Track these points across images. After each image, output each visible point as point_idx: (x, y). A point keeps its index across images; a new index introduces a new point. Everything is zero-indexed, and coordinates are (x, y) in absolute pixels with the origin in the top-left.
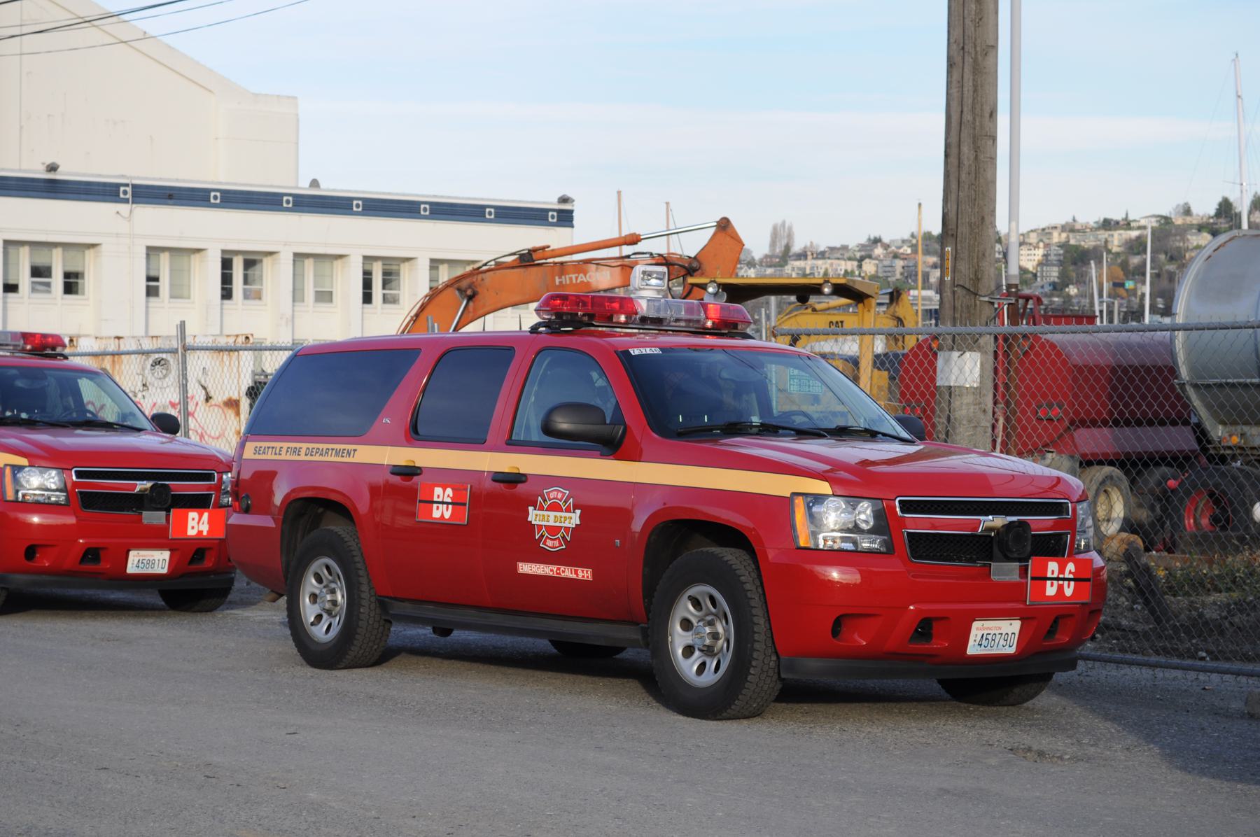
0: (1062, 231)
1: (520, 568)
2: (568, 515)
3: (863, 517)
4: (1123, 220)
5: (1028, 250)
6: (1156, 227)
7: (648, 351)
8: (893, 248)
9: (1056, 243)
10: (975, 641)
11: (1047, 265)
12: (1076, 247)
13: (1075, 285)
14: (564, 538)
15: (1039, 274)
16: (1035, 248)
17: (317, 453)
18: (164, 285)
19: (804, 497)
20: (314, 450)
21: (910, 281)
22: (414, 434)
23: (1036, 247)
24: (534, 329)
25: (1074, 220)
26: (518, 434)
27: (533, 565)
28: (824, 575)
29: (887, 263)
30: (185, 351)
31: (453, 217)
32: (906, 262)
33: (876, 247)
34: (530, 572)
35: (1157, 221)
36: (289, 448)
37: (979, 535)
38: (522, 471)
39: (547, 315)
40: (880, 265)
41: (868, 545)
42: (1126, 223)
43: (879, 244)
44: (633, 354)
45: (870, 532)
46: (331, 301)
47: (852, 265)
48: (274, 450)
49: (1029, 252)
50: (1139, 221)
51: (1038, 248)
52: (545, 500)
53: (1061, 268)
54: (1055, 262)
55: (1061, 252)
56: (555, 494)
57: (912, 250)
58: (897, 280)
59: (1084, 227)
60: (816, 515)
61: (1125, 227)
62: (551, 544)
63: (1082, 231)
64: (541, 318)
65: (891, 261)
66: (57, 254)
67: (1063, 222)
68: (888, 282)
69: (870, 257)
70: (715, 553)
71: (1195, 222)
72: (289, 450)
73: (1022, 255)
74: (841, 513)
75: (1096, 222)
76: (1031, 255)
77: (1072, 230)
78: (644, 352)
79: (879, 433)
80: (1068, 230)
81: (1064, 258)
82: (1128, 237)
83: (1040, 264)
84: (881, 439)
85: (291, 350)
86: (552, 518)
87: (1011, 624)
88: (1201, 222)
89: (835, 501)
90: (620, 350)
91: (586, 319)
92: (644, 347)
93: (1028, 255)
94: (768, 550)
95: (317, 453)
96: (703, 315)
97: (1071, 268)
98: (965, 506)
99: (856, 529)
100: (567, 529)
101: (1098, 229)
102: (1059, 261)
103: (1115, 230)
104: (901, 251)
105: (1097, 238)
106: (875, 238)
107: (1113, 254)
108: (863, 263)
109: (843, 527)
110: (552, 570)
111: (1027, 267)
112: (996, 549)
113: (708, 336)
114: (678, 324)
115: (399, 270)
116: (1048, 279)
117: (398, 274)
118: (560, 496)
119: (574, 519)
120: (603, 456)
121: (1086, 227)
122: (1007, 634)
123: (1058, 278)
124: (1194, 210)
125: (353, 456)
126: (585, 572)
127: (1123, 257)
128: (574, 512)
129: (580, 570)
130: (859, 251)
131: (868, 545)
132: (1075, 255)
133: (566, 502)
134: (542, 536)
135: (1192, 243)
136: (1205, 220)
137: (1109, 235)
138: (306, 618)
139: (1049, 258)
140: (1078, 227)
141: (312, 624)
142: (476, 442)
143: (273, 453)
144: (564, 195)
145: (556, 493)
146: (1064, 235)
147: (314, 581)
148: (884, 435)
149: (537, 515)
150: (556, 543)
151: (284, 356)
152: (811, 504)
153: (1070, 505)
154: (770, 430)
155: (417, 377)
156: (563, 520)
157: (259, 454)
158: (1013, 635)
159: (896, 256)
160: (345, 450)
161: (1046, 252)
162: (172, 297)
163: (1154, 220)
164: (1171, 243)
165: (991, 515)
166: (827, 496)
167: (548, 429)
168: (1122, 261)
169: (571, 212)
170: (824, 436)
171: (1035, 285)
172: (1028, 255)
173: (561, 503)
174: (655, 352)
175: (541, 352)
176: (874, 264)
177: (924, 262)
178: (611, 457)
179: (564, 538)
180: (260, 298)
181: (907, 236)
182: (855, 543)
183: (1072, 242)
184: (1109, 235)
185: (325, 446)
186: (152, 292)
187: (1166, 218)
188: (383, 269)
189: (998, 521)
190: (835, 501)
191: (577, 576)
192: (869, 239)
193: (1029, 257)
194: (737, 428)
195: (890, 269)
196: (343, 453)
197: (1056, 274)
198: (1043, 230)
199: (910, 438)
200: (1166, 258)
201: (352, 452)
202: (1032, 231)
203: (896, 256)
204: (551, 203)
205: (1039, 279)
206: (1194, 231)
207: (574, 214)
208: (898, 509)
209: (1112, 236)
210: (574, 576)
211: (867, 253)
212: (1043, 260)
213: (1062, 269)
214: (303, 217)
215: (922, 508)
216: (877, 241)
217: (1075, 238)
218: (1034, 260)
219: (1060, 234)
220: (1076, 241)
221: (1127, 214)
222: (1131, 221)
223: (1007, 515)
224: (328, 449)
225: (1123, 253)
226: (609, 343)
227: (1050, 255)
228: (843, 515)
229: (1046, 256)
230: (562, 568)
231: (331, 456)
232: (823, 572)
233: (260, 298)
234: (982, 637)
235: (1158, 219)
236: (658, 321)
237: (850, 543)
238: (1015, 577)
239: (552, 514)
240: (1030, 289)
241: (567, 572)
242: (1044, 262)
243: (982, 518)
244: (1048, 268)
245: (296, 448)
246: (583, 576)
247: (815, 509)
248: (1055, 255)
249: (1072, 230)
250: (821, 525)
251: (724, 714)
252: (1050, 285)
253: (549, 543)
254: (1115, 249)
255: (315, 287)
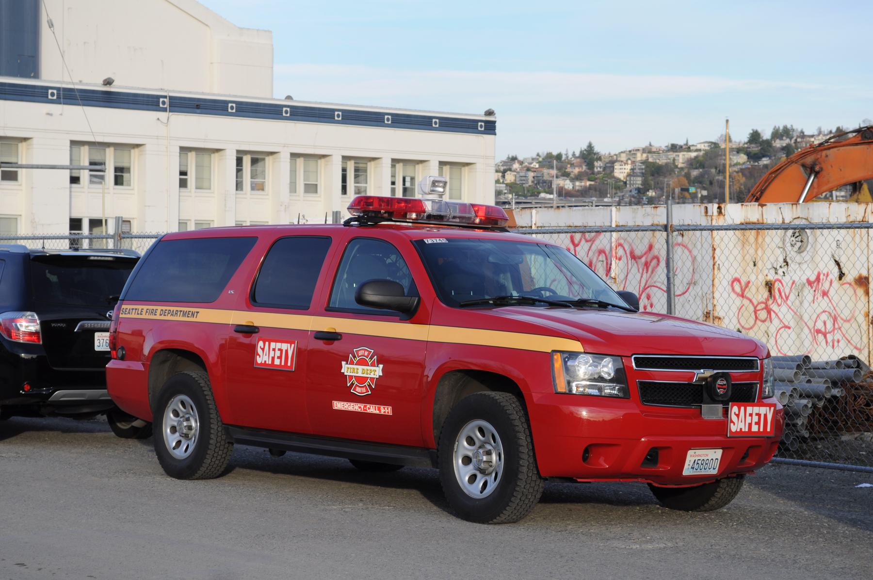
0: (643, 153)
1: (335, 405)
2: (373, 368)
3: (606, 369)
4: (685, 145)
5: (620, 165)
6: (708, 150)
7: (438, 241)
8: (526, 164)
9: (639, 161)
10: (689, 465)
11: (634, 176)
12: (654, 164)
13: (653, 190)
14: (370, 386)
15: (628, 182)
16: (625, 164)
17: (168, 313)
18: (191, 178)
19: (561, 354)
20: (167, 312)
21: (538, 187)
22: (253, 302)
23: (626, 164)
24: (347, 223)
25: (650, 145)
26: (335, 303)
27: (345, 403)
28: (577, 413)
29: (522, 174)
30: (121, 239)
31: (409, 126)
32: (535, 173)
33: (514, 163)
34: (343, 409)
35: (709, 146)
36: (148, 309)
37: (694, 385)
38: (255, 325)
39: (356, 213)
40: (518, 176)
41: (610, 391)
42: (687, 147)
43: (516, 161)
44: (427, 243)
45: (611, 381)
46: (316, 192)
47: (498, 176)
48: (137, 311)
49: (621, 167)
50: (696, 146)
51: (628, 164)
52: (354, 357)
53: (643, 178)
54: (639, 174)
55: (643, 167)
56: (363, 352)
57: (539, 165)
58: (530, 186)
59: (658, 150)
60: (570, 368)
61: (686, 150)
62: (359, 391)
63: (657, 152)
64: (351, 214)
65: (525, 172)
66: (110, 152)
67: (644, 146)
68: (524, 188)
69: (510, 170)
70: (491, 396)
71: (734, 146)
72: (148, 311)
73: (616, 169)
74: (589, 366)
75: (666, 147)
76: (622, 169)
77: (650, 152)
78: (435, 242)
79: (609, 304)
80: (647, 151)
81: (646, 171)
82: (689, 157)
83: (629, 175)
84: (611, 309)
85: (155, 238)
86: (360, 371)
87: (715, 452)
88: (738, 146)
89: (584, 357)
90: (414, 240)
91: (386, 215)
92: (435, 237)
93: (620, 169)
94: (533, 394)
95: (168, 313)
96: (473, 214)
97: (650, 178)
98: (678, 362)
99: (601, 379)
100: (372, 379)
101: (668, 151)
102: (642, 173)
103: (680, 152)
104: (532, 166)
105: (667, 157)
106: (513, 157)
107: (679, 168)
108: (506, 174)
109: (591, 377)
110: (360, 407)
111: (620, 177)
112: (705, 395)
113: (476, 230)
114: (454, 220)
115: (367, 167)
116: (634, 185)
117: (365, 171)
118: (366, 354)
119: (377, 371)
120: (402, 320)
121: (659, 150)
122: (717, 459)
123: (642, 185)
124: (734, 139)
125: (196, 317)
126: (386, 409)
127: (686, 171)
128: (377, 366)
129: (382, 407)
130: (502, 166)
131: (610, 391)
132: (653, 169)
133: (371, 358)
134: (352, 384)
135: (733, 161)
136: (741, 145)
137: (676, 155)
138: (169, 444)
139: (635, 171)
140: (654, 150)
141: (174, 448)
142: (301, 306)
143: (136, 313)
144: (490, 109)
145: (363, 351)
146: (645, 155)
147: (172, 415)
148: (613, 306)
149: (348, 368)
150: (364, 390)
151: (150, 243)
152: (567, 360)
153: (759, 361)
154: (526, 301)
155: (256, 258)
156: (369, 372)
157: (125, 314)
158: (717, 460)
159: (528, 169)
160: (190, 312)
161: (632, 167)
162: (197, 188)
163: (706, 145)
164: (719, 161)
165: (703, 369)
166: (579, 353)
167: (360, 300)
168: (685, 173)
169: (494, 122)
170: (569, 307)
171: (625, 190)
172: (620, 169)
173: (367, 359)
174: (443, 242)
175: (351, 241)
176: (514, 175)
177: (548, 174)
178: (408, 322)
179: (370, 386)
180: (263, 190)
181: (534, 156)
182: (600, 389)
183: (651, 160)
184: (676, 155)
185: (175, 309)
186: (183, 184)
187: (715, 144)
188: (355, 167)
189: (708, 373)
190: (584, 357)
191: (380, 412)
192: (508, 158)
193: (621, 171)
194: (503, 301)
195: (524, 178)
196: (189, 314)
197: (640, 182)
198: (630, 151)
199: (629, 307)
200: (716, 171)
201: (196, 314)
202: (622, 152)
203: (528, 169)
204: (479, 115)
205: (628, 186)
206: (734, 153)
207: (496, 124)
208: (634, 364)
209: (678, 156)
210: (377, 412)
211: (508, 167)
212: (630, 173)
213: (644, 179)
214: (297, 124)
215: (671, 364)
216: (514, 159)
217: (652, 157)
218: (625, 173)
219: (642, 155)
220: (653, 160)
221: (687, 141)
222: (690, 146)
223: (714, 369)
224: (177, 311)
225: (686, 167)
226: (405, 234)
227: (635, 169)
228: (590, 368)
229: (633, 169)
230: (368, 406)
231: (180, 316)
232: (576, 412)
233: (263, 190)
234: (694, 462)
235: (710, 144)
236: (440, 218)
237: (596, 389)
238: (719, 416)
239: (360, 367)
240: (622, 192)
241: (372, 409)
242: (632, 174)
243: (696, 371)
244: (634, 178)
245: (153, 310)
246: (385, 412)
247: (569, 363)
248: (639, 169)
249: (650, 152)
250: (574, 376)
251: (495, 520)
252: (636, 190)
253: (358, 389)
254: (680, 165)
255: (304, 181)
